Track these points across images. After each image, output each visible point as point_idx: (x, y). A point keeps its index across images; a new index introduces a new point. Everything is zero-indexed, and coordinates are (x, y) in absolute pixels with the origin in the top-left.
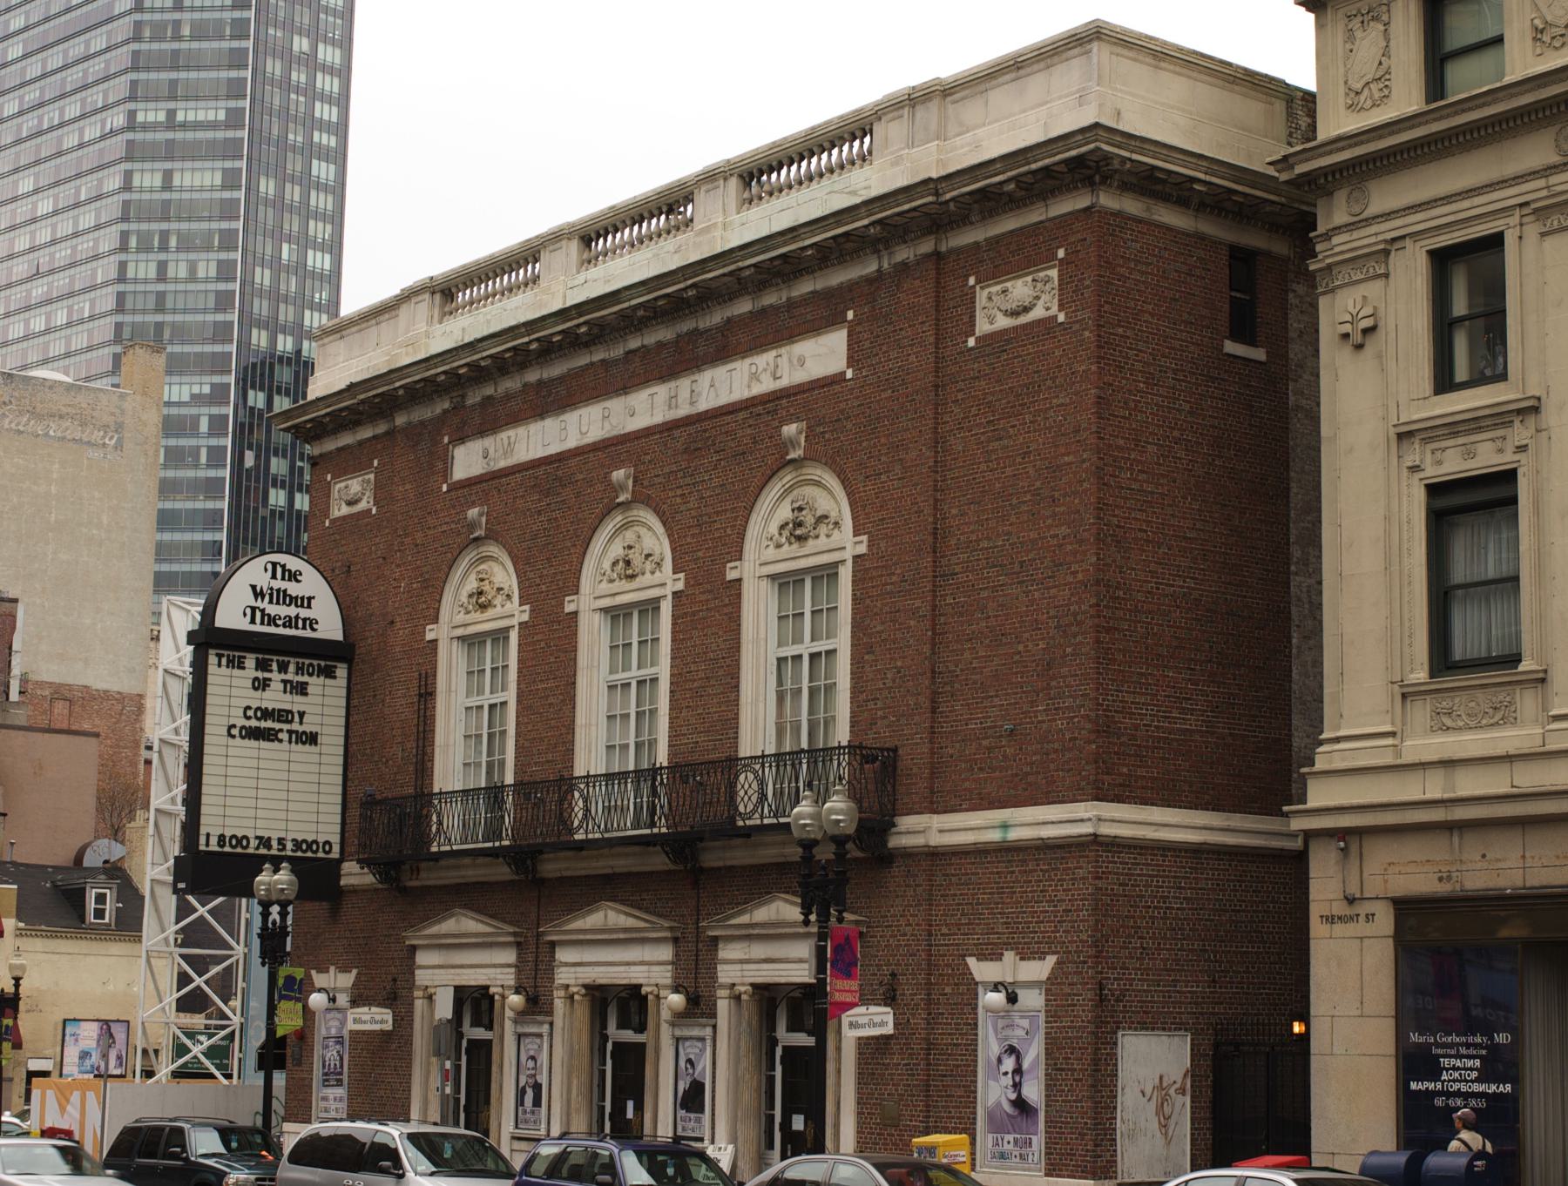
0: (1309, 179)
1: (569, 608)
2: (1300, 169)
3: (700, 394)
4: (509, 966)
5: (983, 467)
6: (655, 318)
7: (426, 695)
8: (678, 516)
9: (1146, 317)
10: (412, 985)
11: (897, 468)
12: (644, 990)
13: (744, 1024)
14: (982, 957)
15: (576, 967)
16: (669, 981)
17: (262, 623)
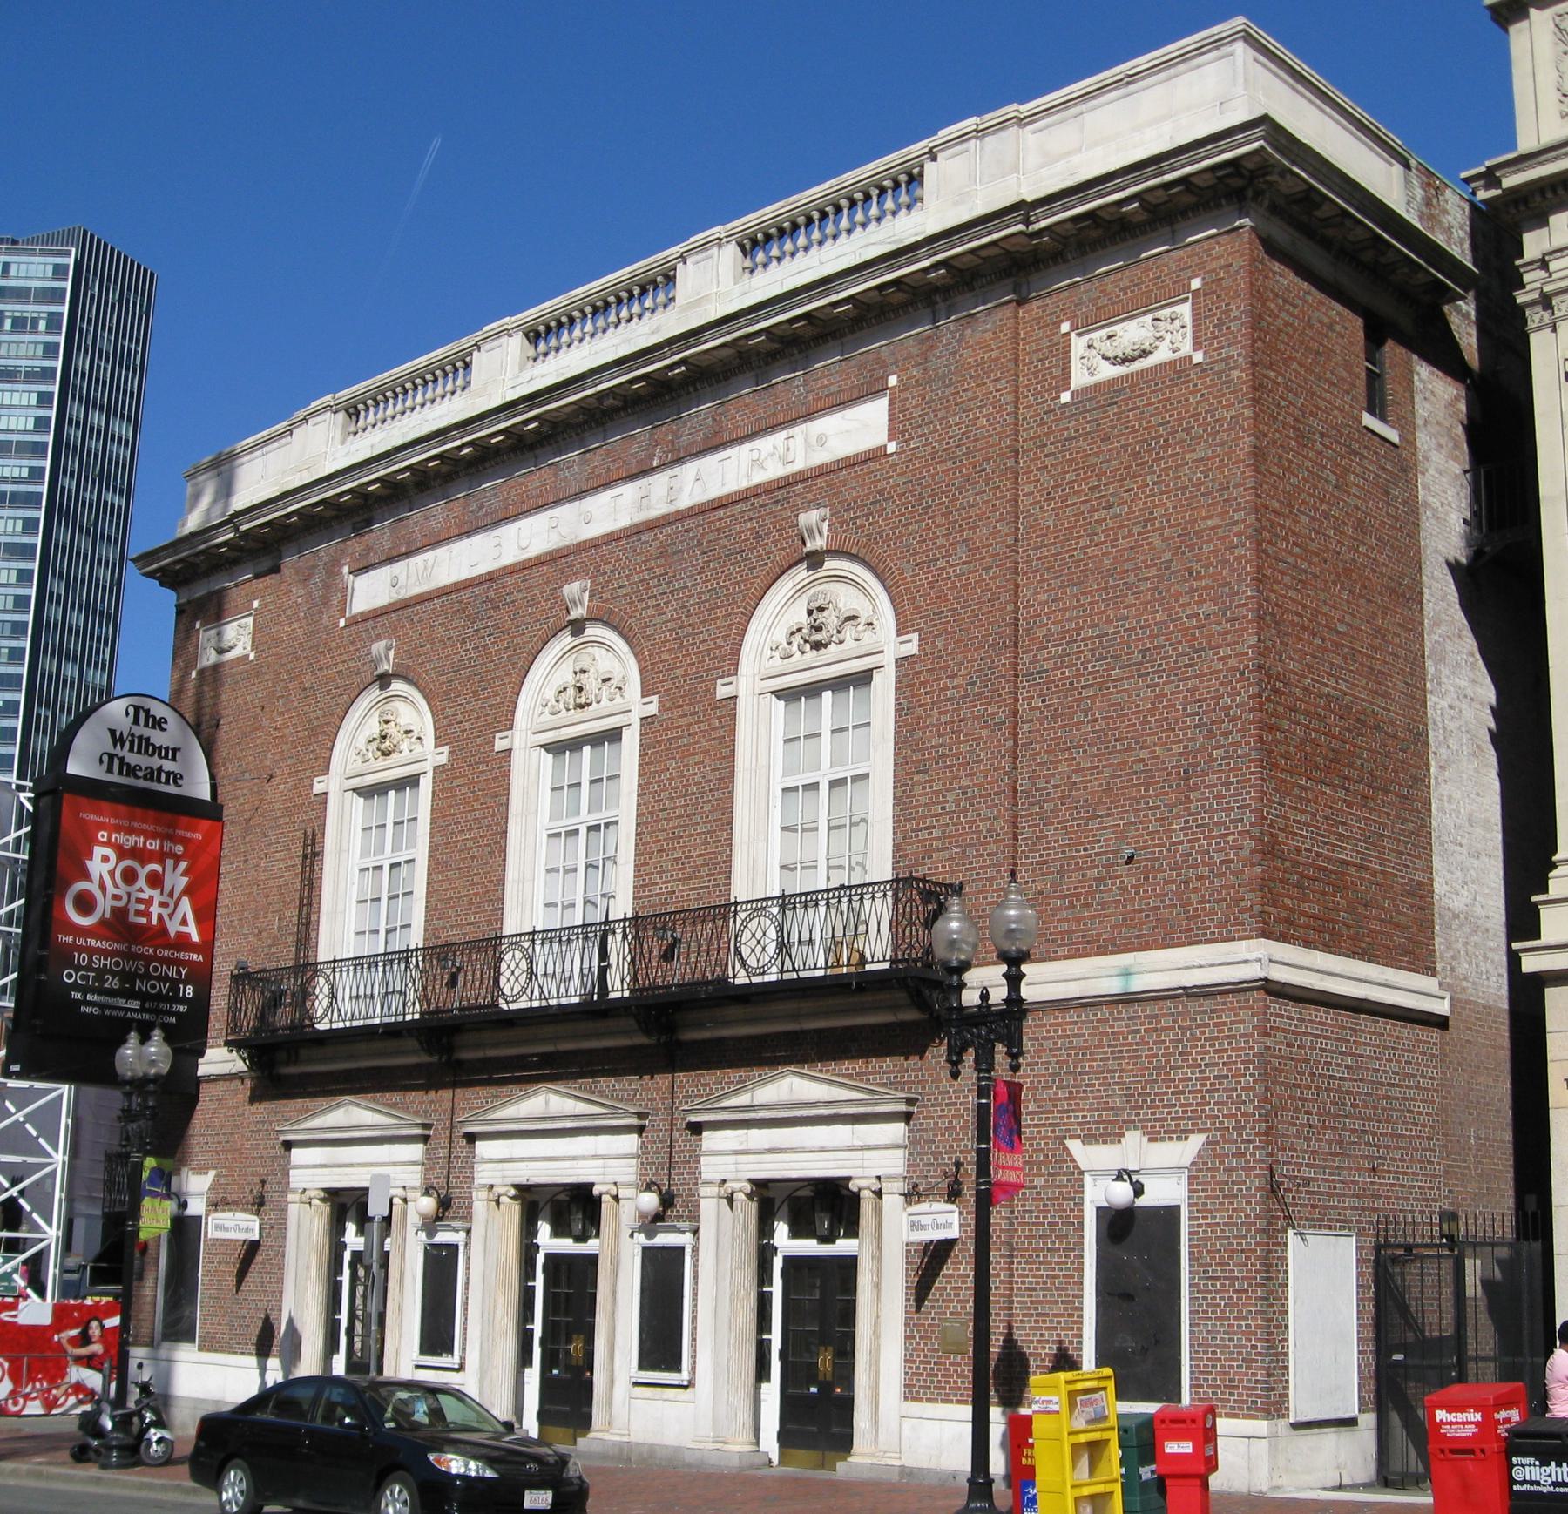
0: (1519, 196)
1: (500, 745)
2: (1509, 181)
3: (681, 490)
4: (414, 1163)
5: (1085, 541)
6: (624, 408)
7: (312, 854)
8: (650, 631)
9: (1295, 365)
10: (285, 1187)
11: (961, 551)
12: (596, 1191)
13: (739, 1227)
14: (1089, 1138)
15: (503, 1164)
16: (632, 1178)
17: (120, 773)
